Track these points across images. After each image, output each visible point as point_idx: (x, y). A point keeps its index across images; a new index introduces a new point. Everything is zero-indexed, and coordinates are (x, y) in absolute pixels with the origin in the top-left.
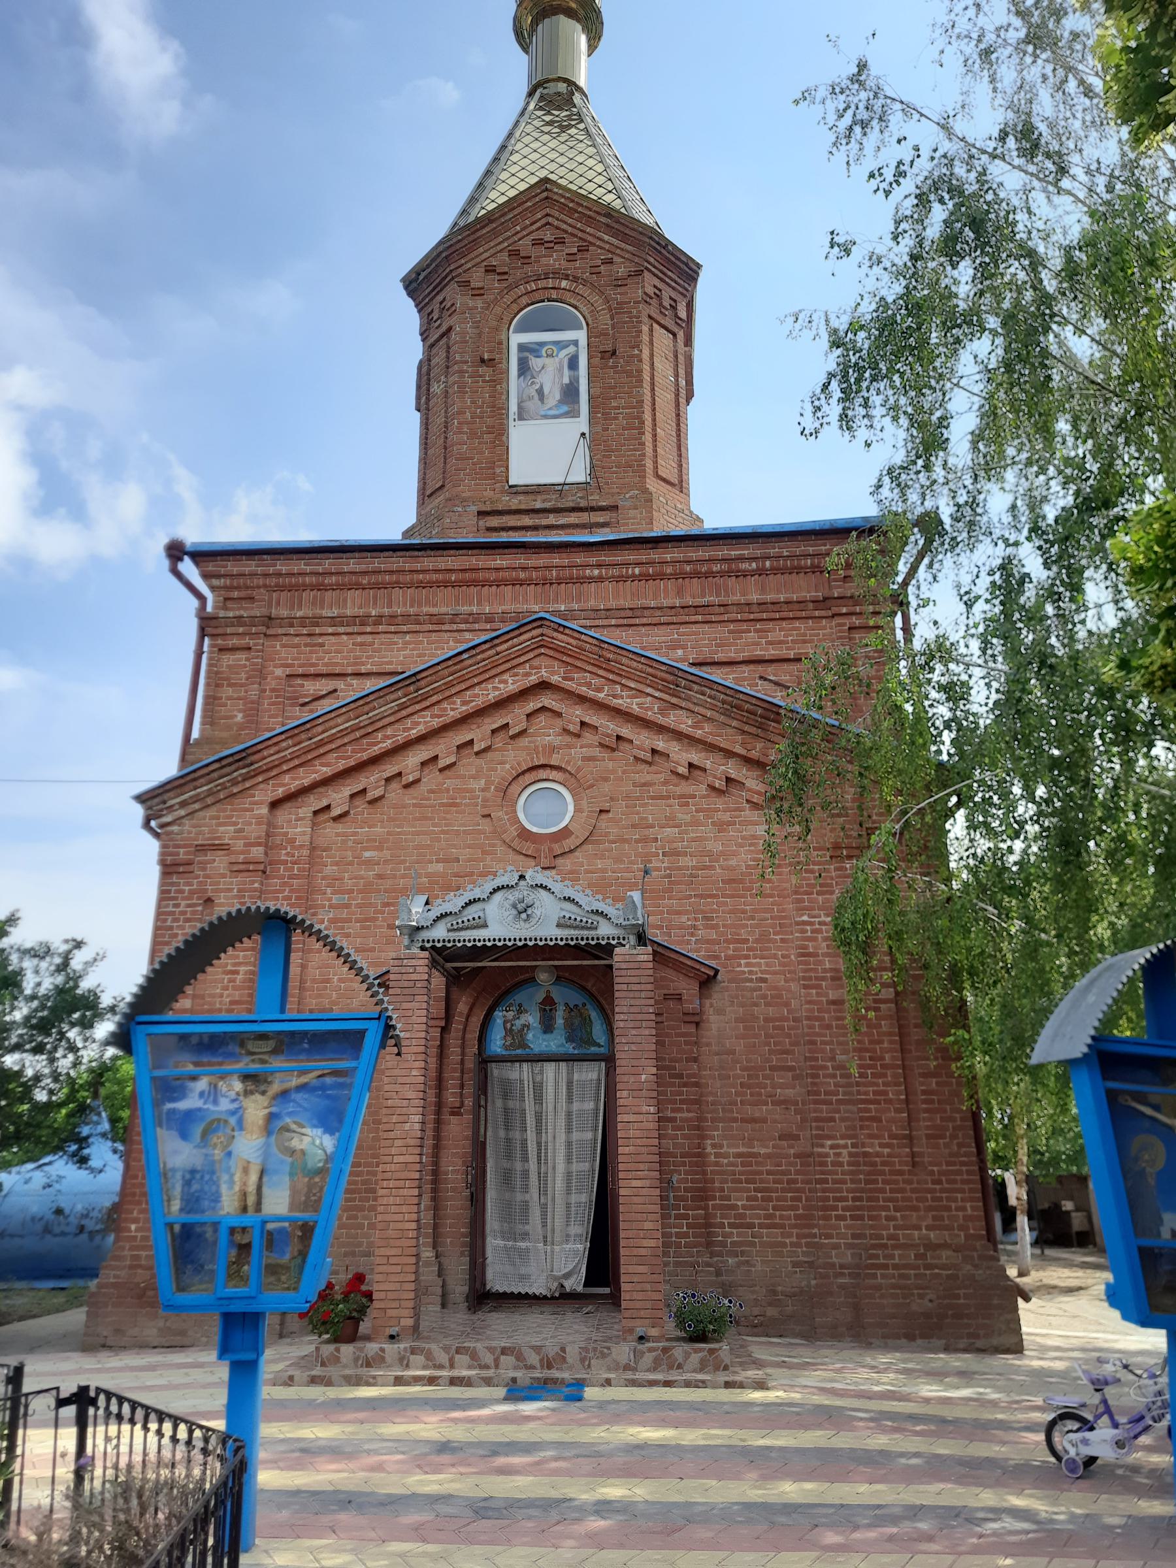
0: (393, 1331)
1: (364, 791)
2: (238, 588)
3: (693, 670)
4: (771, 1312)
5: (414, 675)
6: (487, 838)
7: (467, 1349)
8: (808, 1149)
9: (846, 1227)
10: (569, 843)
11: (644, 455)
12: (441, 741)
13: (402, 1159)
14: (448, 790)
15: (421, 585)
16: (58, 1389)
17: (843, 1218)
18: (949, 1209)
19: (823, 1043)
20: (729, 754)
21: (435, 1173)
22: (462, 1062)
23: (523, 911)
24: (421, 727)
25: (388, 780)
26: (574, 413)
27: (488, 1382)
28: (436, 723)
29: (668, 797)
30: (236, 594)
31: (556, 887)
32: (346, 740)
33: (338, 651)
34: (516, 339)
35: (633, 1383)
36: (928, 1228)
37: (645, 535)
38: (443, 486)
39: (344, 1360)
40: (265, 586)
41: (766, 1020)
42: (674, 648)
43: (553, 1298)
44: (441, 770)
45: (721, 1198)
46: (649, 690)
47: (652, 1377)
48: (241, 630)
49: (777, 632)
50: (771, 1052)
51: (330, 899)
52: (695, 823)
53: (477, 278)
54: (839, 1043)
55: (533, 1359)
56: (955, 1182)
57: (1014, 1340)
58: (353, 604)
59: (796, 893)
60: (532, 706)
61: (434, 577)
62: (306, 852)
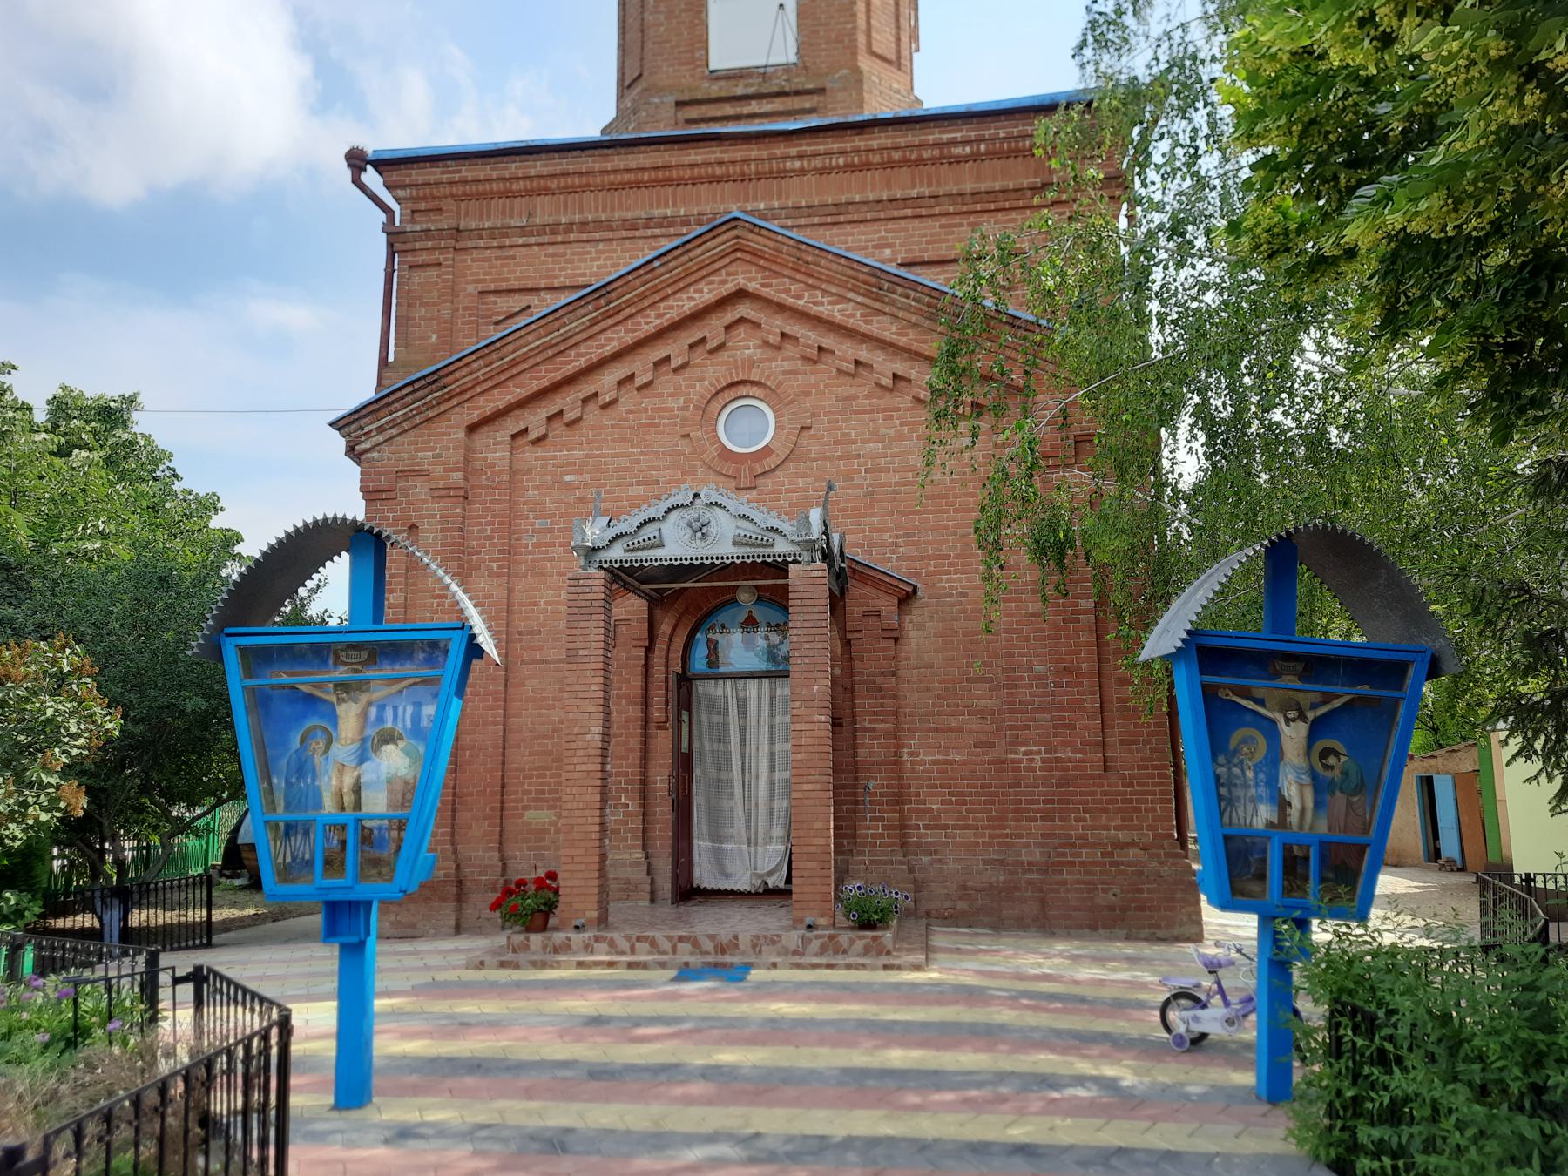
0: (578, 922)
1: (560, 413)
2: (424, 198)
3: (902, 272)
4: (962, 905)
5: (604, 286)
6: (686, 459)
7: (604, 939)
8: (1003, 756)
11: (855, 28)
12: (638, 358)
13: (584, 767)
14: (646, 410)
16: (174, 968)
18: (1138, 810)
23: (700, 530)
24: (615, 343)
25: (585, 401)
27: (663, 965)
28: (629, 339)
29: (871, 411)
30: (423, 206)
32: (538, 359)
33: (530, 265)
35: (798, 966)
36: (1116, 828)
37: (851, 119)
38: (640, 76)
39: (533, 947)
40: (452, 196)
41: (965, 634)
42: (880, 247)
43: (757, 894)
44: (639, 389)
45: (917, 802)
46: (851, 295)
47: (816, 960)
48: (430, 244)
52: (900, 437)
55: (708, 945)
56: (1146, 785)
57: (1194, 930)
58: (545, 211)
60: (730, 316)
61: (627, 177)
62: (505, 477)
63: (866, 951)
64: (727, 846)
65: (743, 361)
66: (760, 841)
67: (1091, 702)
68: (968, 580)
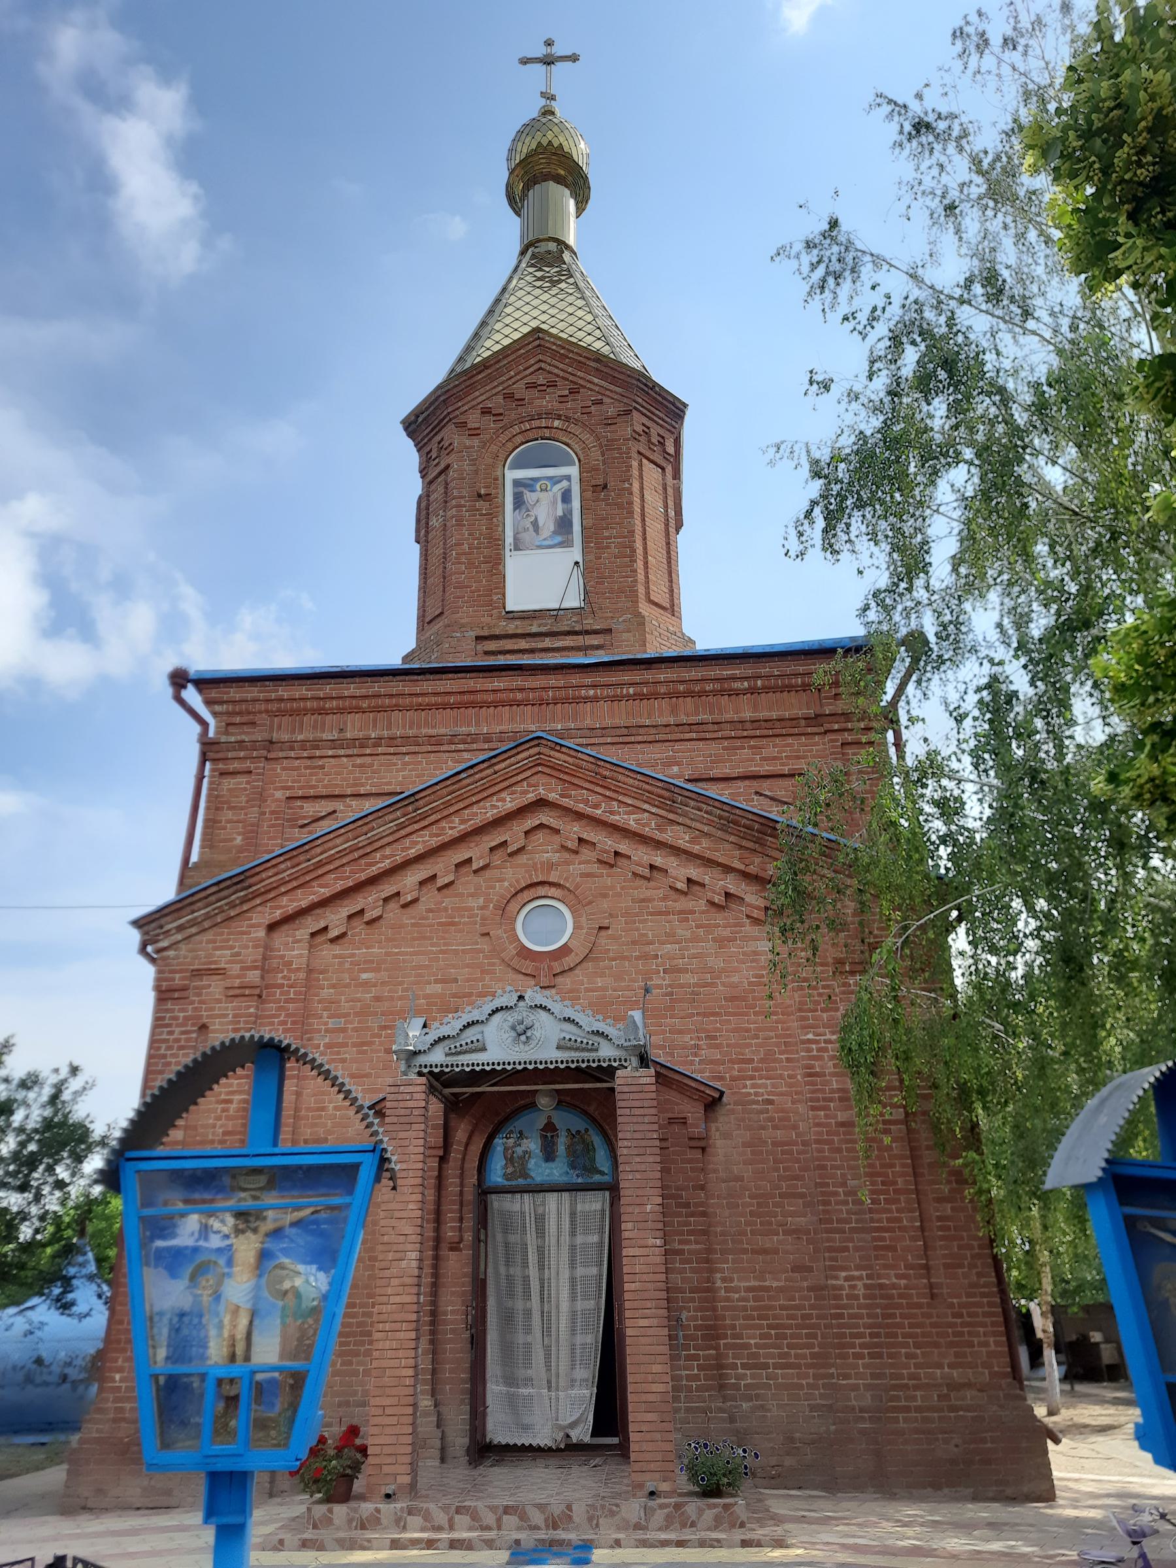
1: (362, 912)
2: (240, 713)
3: (689, 786)
4: (789, 1461)
6: (486, 957)
7: (467, 1508)
9: (865, 1366)
10: (569, 961)
12: (440, 859)
13: (397, 1299)
14: (446, 909)
15: (420, 708)
17: (861, 1356)
19: (833, 1167)
20: (728, 869)
21: (434, 1314)
22: (461, 1193)
23: (522, 1033)
24: (420, 846)
26: (567, 544)
27: (490, 1544)
28: (434, 842)
29: (667, 913)
30: (238, 720)
31: (556, 1007)
32: (344, 861)
33: (338, 773)
34: (511, 475)
35: (644, 1544)
37: (639, 656)
39: (336, 1522)
40: (267, 711)
41: (775, 1144)
43: (559, 1450)
45: (734, 1337)
46: (646, 806)
47: (663, 1536)
48: (242, 754)
49: (771, 748)
50: (780, 1178)
51: (326, 1024)
52: (695, 939)
53: (474, 419)
54: (850, 1168)
55: (537, 1518)
56: (976, 1315)
58: (354, 727)
59: (800, 1010)
60: (530, 823)
61: (433, 699)
62: (302, 975)
63: (717, 1524)
64: (524, 1391)
65: (542, 863)
66: (562, 1383)
67: (909, 1220)
68: (773, 1086)
